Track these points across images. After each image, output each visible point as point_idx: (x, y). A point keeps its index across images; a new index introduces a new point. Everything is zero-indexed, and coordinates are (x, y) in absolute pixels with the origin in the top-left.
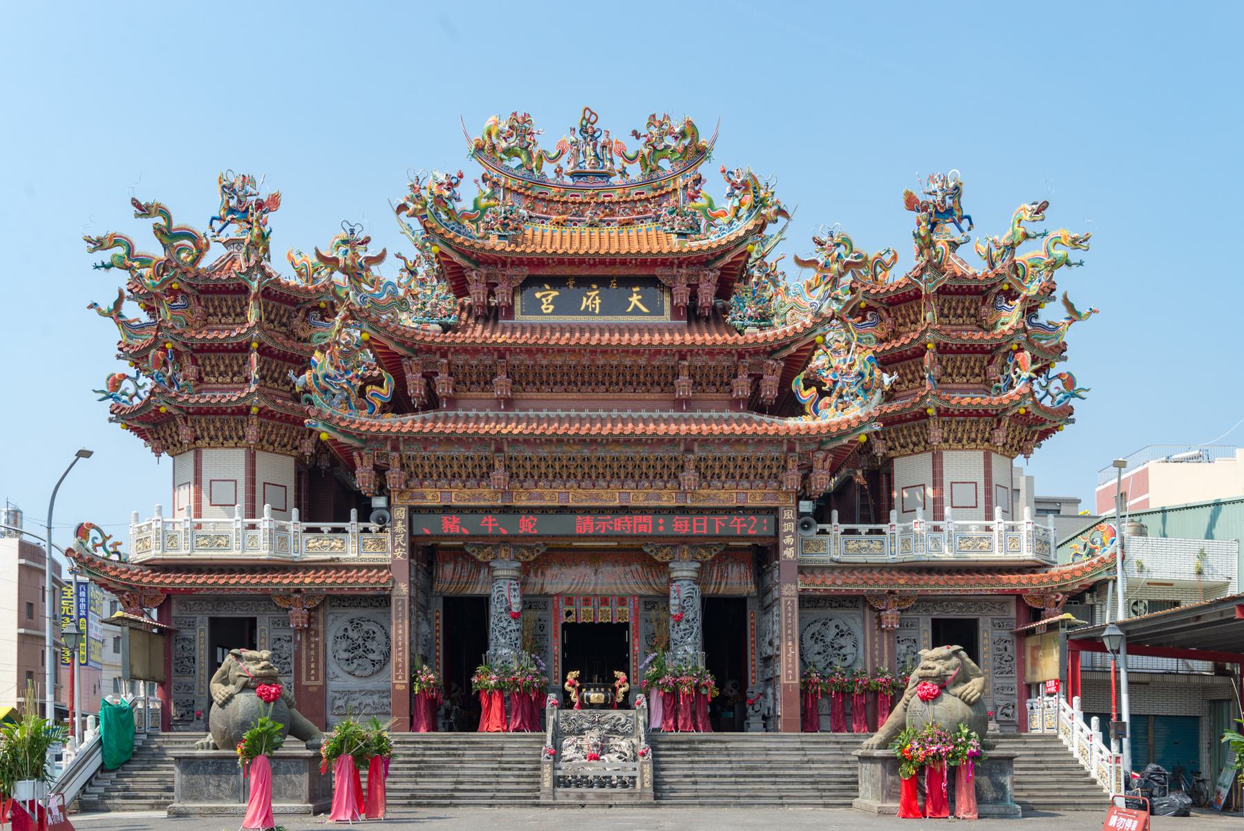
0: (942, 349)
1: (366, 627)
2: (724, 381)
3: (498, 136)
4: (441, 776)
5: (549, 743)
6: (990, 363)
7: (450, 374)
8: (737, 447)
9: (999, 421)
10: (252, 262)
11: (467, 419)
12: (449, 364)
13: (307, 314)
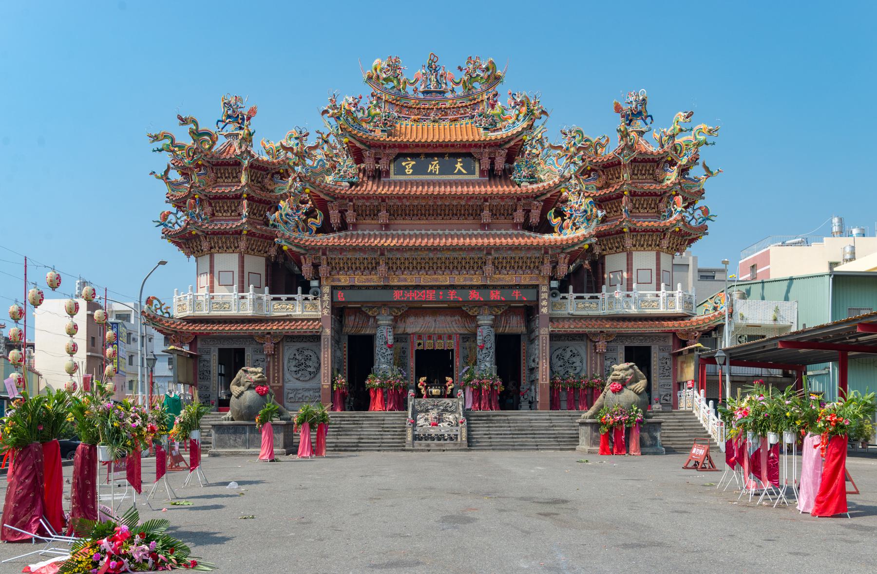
0: (633, 194)
1: (306, 353)
2: (509, 213)
3: (381, 71)
4: (351, 435)
5: (410, 416)
6: (660, 201)
7: (354, 211)
8: (516, 252)
9: (665, 235)
10: (243, 148)
11: (364, 236)
12: (354, 205)
13: (272, 176)
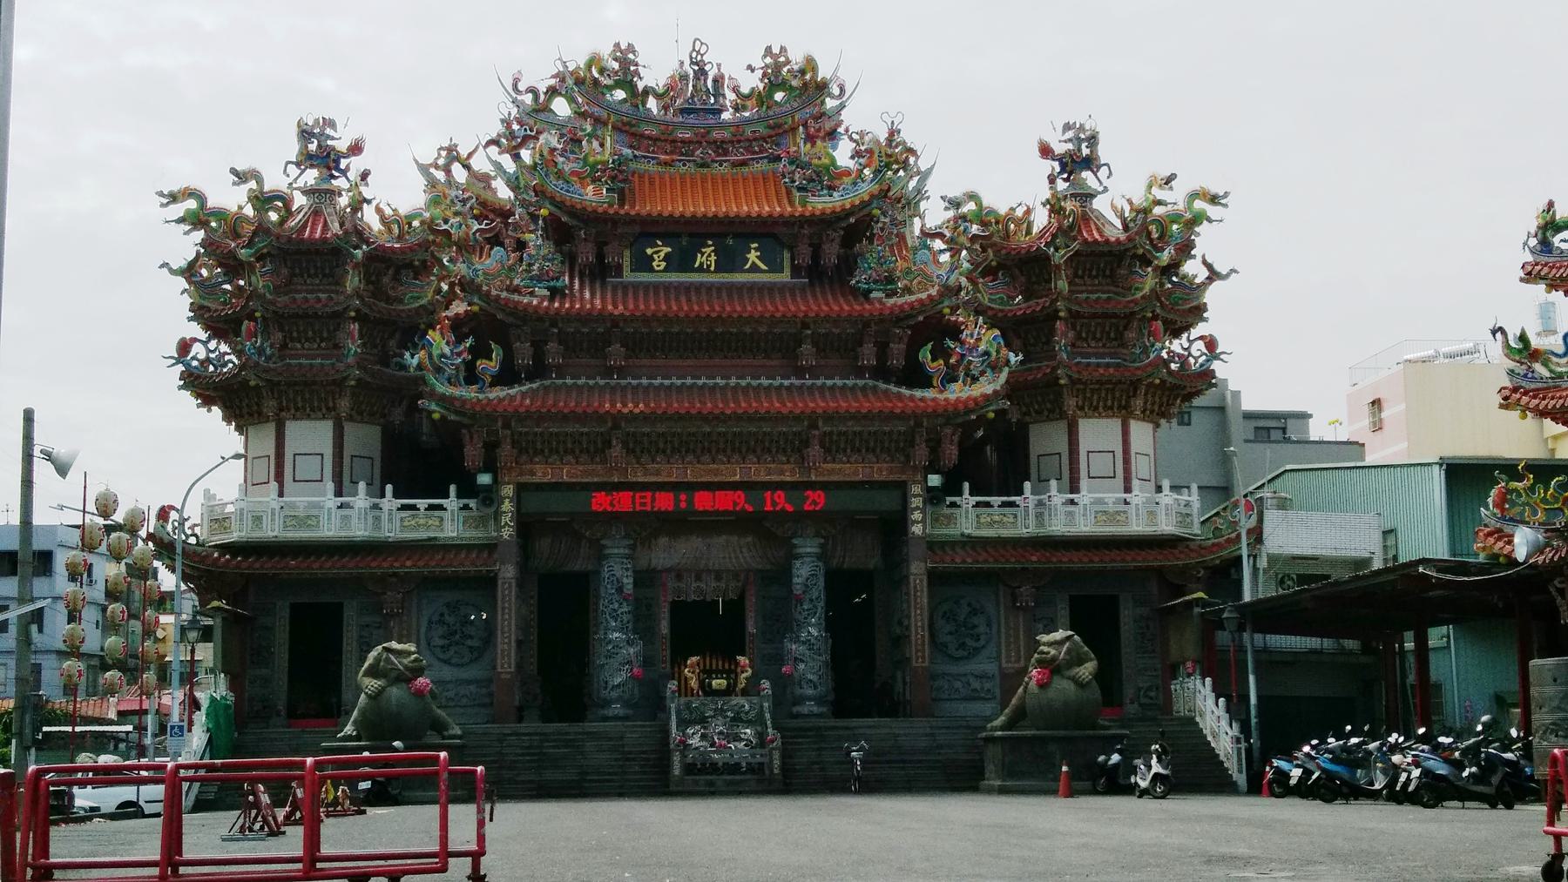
0: (1074, 316)
6: (1125, 328)
9: (1135, 390)
13: (397, 272)
